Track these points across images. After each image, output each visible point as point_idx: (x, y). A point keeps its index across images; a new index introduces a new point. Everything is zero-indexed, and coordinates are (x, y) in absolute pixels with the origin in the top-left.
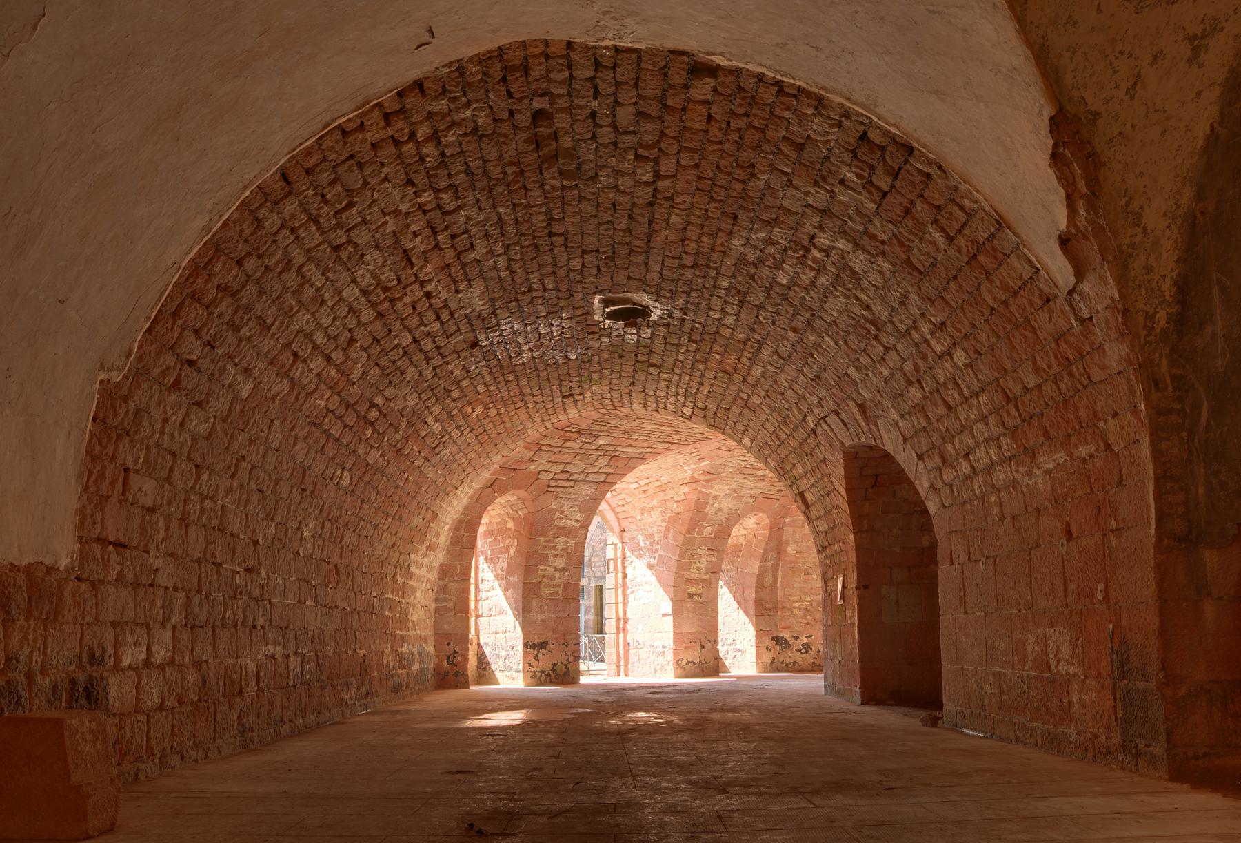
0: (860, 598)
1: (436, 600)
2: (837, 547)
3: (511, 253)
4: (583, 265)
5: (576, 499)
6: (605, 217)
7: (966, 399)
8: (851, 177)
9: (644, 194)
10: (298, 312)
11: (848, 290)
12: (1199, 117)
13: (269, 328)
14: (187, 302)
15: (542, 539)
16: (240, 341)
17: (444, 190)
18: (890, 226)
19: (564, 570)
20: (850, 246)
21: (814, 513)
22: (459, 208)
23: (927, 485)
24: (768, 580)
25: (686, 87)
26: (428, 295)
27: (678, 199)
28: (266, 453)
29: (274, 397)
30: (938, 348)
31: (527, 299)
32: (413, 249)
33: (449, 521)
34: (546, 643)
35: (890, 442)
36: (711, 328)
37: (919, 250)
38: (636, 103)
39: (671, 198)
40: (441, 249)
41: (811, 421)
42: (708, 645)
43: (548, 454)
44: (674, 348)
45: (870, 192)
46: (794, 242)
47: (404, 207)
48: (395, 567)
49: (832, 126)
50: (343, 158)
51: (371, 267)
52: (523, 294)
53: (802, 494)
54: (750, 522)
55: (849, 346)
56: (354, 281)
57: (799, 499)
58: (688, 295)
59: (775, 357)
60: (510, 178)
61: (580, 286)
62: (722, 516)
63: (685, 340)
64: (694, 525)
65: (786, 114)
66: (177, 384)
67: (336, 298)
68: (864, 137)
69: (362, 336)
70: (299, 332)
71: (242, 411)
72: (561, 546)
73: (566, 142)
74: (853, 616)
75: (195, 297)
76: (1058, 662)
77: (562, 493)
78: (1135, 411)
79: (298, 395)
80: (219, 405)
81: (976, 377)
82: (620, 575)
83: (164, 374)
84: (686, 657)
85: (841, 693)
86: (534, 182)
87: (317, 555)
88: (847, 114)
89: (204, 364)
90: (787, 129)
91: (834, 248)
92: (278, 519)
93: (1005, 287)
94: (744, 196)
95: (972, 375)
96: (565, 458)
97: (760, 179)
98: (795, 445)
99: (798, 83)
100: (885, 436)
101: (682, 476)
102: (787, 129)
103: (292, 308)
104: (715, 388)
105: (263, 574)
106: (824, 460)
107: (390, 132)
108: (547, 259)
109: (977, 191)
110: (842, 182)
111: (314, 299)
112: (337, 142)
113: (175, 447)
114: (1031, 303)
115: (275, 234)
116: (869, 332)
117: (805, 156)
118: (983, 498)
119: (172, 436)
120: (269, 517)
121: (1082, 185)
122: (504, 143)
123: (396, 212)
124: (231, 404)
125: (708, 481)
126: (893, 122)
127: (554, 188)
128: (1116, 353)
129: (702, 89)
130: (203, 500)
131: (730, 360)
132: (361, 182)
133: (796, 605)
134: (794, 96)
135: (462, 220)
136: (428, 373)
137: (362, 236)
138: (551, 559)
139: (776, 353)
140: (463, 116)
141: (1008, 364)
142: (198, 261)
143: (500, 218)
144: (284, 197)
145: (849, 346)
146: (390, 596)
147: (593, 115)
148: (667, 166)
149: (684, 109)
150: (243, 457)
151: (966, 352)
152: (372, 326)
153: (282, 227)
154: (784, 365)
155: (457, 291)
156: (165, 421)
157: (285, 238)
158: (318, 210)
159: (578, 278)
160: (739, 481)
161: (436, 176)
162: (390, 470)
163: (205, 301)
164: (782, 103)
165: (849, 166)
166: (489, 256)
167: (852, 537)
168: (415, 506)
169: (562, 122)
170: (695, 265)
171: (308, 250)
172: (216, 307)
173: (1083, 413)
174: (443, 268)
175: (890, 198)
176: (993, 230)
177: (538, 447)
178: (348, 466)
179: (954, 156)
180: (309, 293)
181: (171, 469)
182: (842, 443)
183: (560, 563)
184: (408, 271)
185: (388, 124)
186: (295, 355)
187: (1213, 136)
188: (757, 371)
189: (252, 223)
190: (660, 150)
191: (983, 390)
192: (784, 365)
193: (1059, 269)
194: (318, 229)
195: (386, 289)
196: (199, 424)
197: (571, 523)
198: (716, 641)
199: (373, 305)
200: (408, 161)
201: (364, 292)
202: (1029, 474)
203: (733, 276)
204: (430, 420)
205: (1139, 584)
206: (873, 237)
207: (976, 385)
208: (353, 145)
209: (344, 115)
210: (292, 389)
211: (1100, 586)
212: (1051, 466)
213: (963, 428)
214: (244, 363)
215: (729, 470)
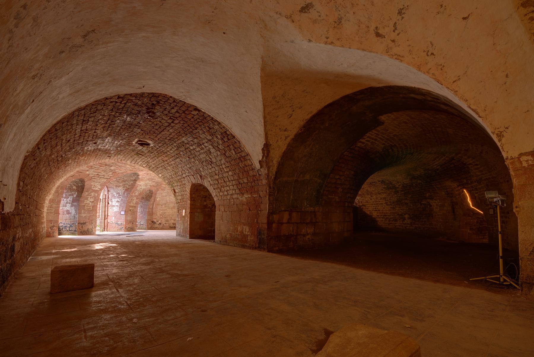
1: (47, 210)
6: (153, 125)
8: (219, 137)
9: (167, 124)
12: (284, 148)
19: (93, 202)
21: (177, 194)
30: (226, 171)
35: (206, 184)
41: (184, 175)
42: (134, 223)
68: (225, 132)
69: (72, 141)
77: (96, 180)
78: (266, 192)
82: (107, 203)
84: (128, 226)
85: (182, 236)
88: (224, 127)
93: (245, 165)
96: (99, 171)
101: (132, 179)
117: (210, 131)
121: (266, 154)
128: (264, 182)
129: (195, 113)
131: (166, 158)
141: (241, 177)
160: (148, 182)
167: (189, 202)
173: (256, 190)
177: (91, 167)
179: (243, 142)
183: (92, 200)
187: (285, 151)
188: (173, 162)
193: (258, 166)
195: (87, 130)
197: (97, 189)
205: (263, 219)
207: (233, 179)
213: (227, 186)
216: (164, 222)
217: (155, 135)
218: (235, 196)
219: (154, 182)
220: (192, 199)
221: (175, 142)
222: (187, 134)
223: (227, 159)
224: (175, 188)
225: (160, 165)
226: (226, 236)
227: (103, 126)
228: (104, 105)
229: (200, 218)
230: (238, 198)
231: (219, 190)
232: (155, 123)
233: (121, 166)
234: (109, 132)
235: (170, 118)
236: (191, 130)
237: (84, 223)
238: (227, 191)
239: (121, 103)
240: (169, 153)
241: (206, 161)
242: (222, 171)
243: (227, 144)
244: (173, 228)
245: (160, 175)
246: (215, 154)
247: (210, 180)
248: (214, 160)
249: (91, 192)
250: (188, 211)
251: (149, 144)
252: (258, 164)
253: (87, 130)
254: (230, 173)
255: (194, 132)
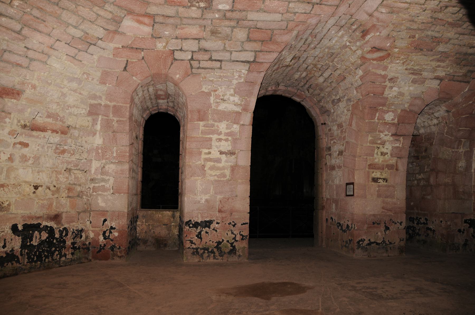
15: (202, 123)
34: (210, 222)
138: (214, 143)
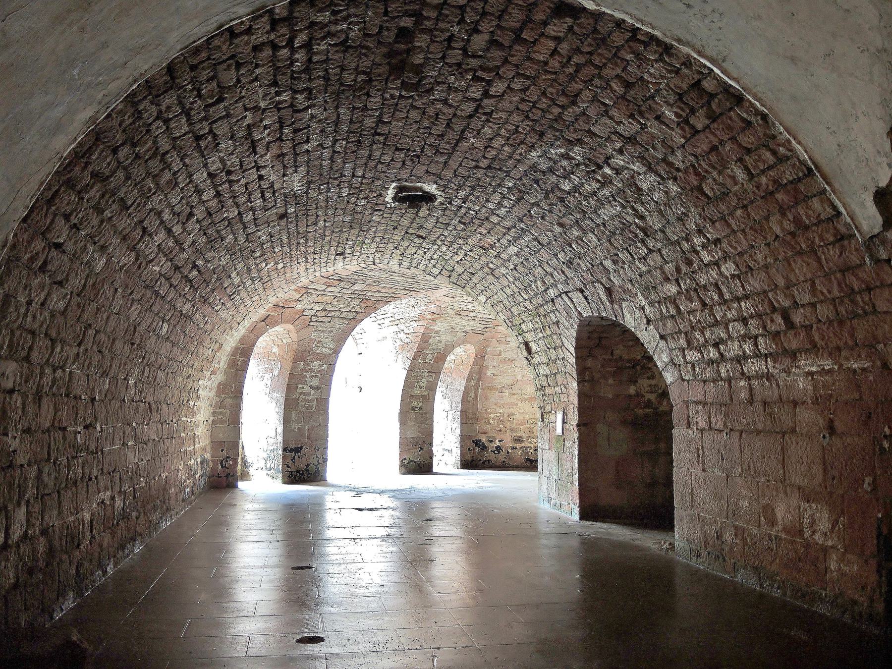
0: (580, 434)
2: (558, 389)
3: (338, 146)
4: (392, 160)
5: (331, 331)
6: (426, 123)
7: (725, 301)
9: (468, 108)
10: (154, 193)
11: (628, 202)
13: (128, 209)
14: (63, 189)
16: (102, 222)
17: (301, 92)
18: (692, 158)
19: (318, 388)
20: (645, 169)
21: (536, 359)
22: (309, 107)
23: (666, 359)
24: (472, 394)
25: (545, 24)
26: (260, 178)
27: (495, 116)
28: (108, 318)
29: (121, 268)
30: (707, 259)
31: (336, 182)
32: (259, 140)
33: (229, 349)
34: (301, 448)
35: (630, 320)
36: (482, 216)
37: (714, 180)
38: (492, 32)
39: (490, 114)
40: (282, 141)
41: (552, 293)
43: (314, 296)
44: (442, 226)
45: (683, 129)
46: (589, 160)
47: (263, 104)
48: (189, 393)
49: (670, 72)
50: (224, 58)
51: (222, 155)
52: (335, 179)
53: (527, 345)
54: (459, 351)
55: (611, 244)
56: (205, 165)
57: (523, 347)
58: (473, 189)
59: (535, 243)
60: (358, 85)
61: (383, 175)
62: (441, 346)
63: (455, 222)
64: (418, 354)
65: (629, 57)
66: (43, 269)
67: (188, 180)
68: (696, 86)
69: (199, 212)
70: (151, 210)
71: (94, 284)
72: (316, 369)
73: (418, 59)
74: (573, 446)
75: (70, 184)
76: (814, 532)
79: (141, 263)
80: (75, 283)
81: (743, 286)
83: (32, 259)
84: (408, 457)
86: (378, 90)
87: (137, 398)
88: (688, 63)
89: (69, 247)
90: (624, 69)
91: (627, 168)
92: (112, 374)
93: (797, 221)
94: (558, 118)
95: (739, 284)
97: (579, 107)
98: (530, 307)
99: (656, 33)
100: (628, 316)
102: (624, 69)
103: (150, 190)
104: (467, 258)
105: (98, 428)
106: (557, 323)
107: (272, 37)
108: (365, 153)
109: (799, 143)
110: (658, 118)
111: (169, 182)
112: (224, 42)
113: (36, 325)
114: (822, 239)
115: (151, 124)
116: (636, 235)
118: (729, 380)
119: (34, 317)
120: (105, 374)
122: (365, 55)
123: (256, 108)
124: (86, 279)
125: (433, 319)
126: (735, 76)
127: (392, 97)
130: (54, 371)
131: (490, 240)
132: (235, 80)
133: (492, 415)
134: (643, 42)
135: (307, 117)
136: (242, 240)
137: (222, 128)
138: (308, 379)
139: (536, 240)
140: (339, 28)
142: (78, 149)
143: (338, 117)
144: (166, 92)
145: (611, 244)
146: (184, 419)
147: (451, 39)
148: (498, 87)
149: (534, 43)
150: (90, 325)
151: (737, 266)
152: (210, 203)
153: (157, 118)
154: (540, 249)
155: (284, 175)
156: (29, 303)
157: (158, 128)
158: (192, 103)
159: (385, 169)
161: (299, 79)
162: (197, 317)
163: (78, 187)
164: (630, 47)
165: (672, 106)
166: (320, 148)
167: (575, 385)
168: (208, 341)
169: (421, 41)
170: (489, 167)
171: (174, 139)
172: (87, 192)
174: (279, 156)
175: (701, 136)
176: (801, 174)
178: (167, 318)
180: (167, 176)
181: (31, 348)
182: (580, 313)
183: (315, 382)
184: (252, 158)
185: (273, 29)
186: (144, 230)
188: (513, 250)
189: (133, 114)
190: (498, 74)
191: (746, 297)
192: (540, 249)
194: (187, 121)
195: (229, 173)
196: (57, 303)
198: (431, 444)
199: (215, 186)
200: (280, 64)
201: (211, 175)
202: (788, 372)
203: (520, 179)
204: (233, 275)
206: (670, 164)
207: (740, 292)
208: (237, 46)
209: (239, 18)
210: (137, 260)
211: (868, 480)
212: (814, 369)
213: (717, 323)
214: (102, 242)
215: (450, 311)
216: (508, 443)
217: (442, 159)
218: (754, 366)
219: (474, 319)
220: (584, 375)
221: (508, 174)
222: (542, 135)
223: (711, 211)
224: (529, 337)
225: (477, 266)
226: (719, 536)
227: (274, 150)
228: (239, 66)
229: (617, 441)
230: (769, 376)
231: (683, 342)
232: (431, 111)
233: (378, 282)
234: (303, 169)
235: (476, 79)
236: (556, 111)
237: (298, 450)
238: (716, 345)
239: (290, 43)
240: (495, 219)
241: (626, 226)
242: (689, 263)
243: (703, 143)
244: (530, 465)
245: (483, 298)
246: (656, 196)
247: (643, 302)
248: (655, 222)
249: (312, 361)
250: (574, 419)
251: (429, 198)
252: (872, 210)
253: (229, 173)
254: (729, 268)
255: (569, 114)
